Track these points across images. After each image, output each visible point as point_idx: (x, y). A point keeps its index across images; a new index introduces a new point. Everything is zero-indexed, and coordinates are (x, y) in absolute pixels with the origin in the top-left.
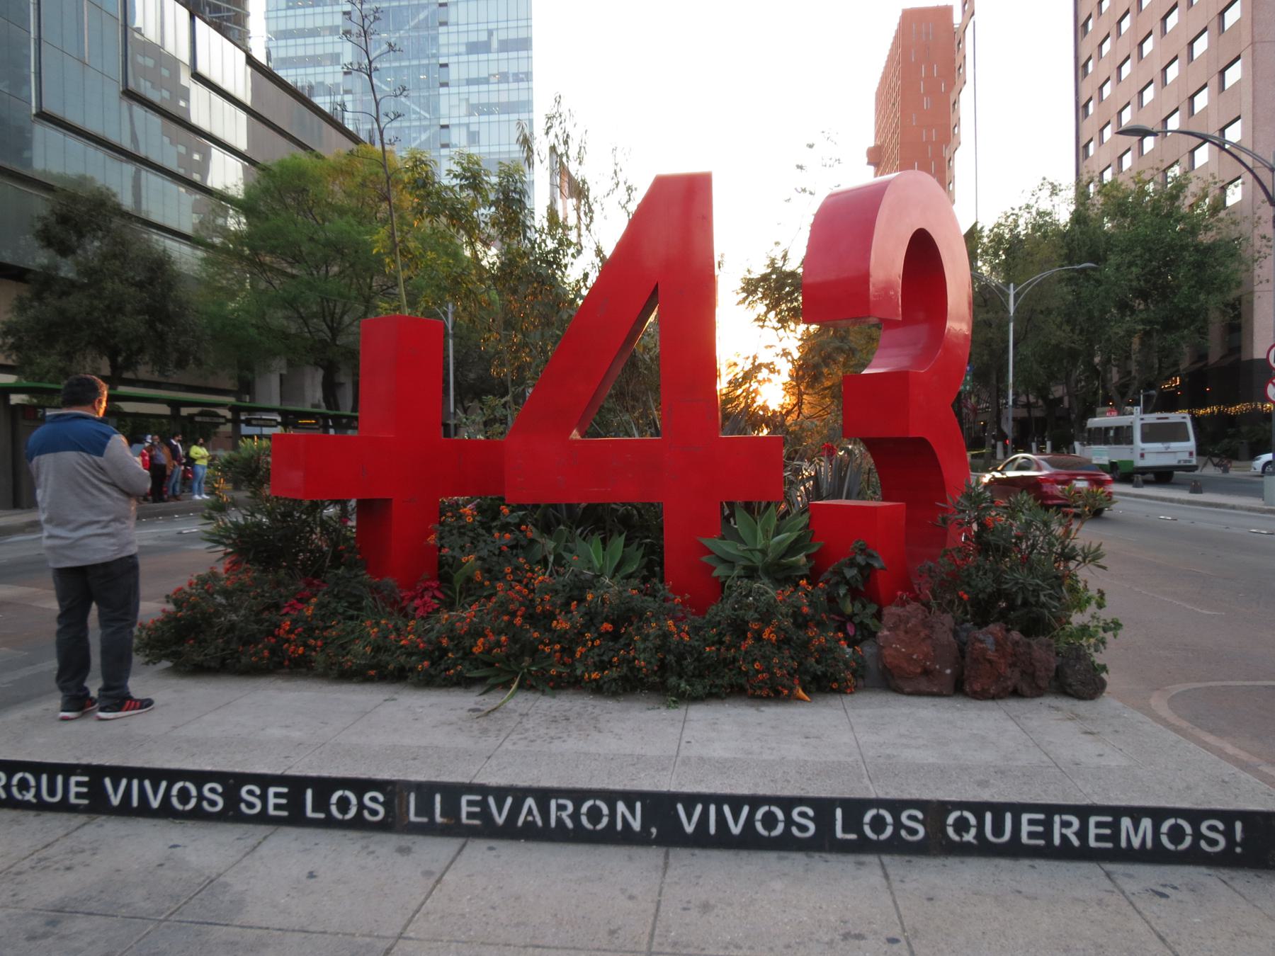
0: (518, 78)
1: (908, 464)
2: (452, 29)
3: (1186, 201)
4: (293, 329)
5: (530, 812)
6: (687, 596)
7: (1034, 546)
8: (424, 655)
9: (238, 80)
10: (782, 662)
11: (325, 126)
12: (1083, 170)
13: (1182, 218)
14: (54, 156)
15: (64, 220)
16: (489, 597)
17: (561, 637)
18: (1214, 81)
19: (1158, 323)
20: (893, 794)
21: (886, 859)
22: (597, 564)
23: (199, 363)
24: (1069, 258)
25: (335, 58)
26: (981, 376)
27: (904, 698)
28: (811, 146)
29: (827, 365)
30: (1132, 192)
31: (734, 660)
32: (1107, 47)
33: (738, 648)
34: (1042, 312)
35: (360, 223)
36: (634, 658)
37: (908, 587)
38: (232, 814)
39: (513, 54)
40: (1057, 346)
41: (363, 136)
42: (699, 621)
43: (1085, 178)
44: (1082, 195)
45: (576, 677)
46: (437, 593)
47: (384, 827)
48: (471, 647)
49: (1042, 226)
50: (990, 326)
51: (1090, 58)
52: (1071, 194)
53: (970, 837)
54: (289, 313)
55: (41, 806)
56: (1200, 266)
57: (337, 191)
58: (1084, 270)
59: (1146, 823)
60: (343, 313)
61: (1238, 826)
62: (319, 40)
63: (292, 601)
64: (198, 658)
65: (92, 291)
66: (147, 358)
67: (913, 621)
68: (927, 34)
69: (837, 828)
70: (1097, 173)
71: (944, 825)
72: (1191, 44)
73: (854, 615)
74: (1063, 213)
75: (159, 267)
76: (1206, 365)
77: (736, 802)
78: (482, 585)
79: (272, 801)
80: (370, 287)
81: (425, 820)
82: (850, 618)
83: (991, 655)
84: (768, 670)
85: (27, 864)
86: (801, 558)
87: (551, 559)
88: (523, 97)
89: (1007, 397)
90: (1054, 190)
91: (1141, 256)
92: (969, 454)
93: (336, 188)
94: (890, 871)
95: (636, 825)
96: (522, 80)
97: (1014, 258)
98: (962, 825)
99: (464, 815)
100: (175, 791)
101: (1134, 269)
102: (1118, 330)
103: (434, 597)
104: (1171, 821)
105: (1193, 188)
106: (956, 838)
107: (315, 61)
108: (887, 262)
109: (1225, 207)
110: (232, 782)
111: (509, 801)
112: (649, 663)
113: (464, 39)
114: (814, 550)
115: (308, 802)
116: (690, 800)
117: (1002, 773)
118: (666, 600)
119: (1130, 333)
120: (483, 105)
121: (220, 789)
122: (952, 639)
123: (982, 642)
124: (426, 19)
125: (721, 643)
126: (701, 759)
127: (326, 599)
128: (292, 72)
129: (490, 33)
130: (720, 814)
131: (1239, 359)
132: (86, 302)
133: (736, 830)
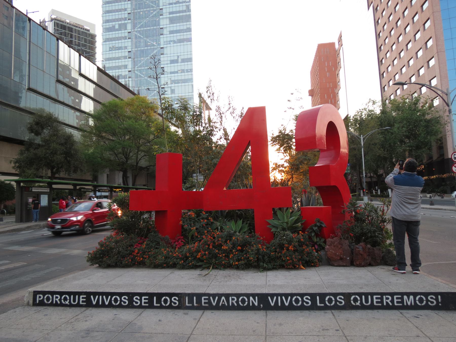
0: (187, 71)
1: (330, 193)
2: (165, 56)
3: (420, 105)
4: (112, 158)
5: (223, 301)
6: (264, 237)
7: (372, 219)
8: (181, 259)
9: (93, 74)
10: (296, 257)
11: (123, 89)
12: (383, 96)
13: (419, 111)
14: (30, 102)
15: (37, 124)
16: (200, 241)
17: (225, 251)
18: (426, 65)
19: (414, 147)
20: (334, 291)
21: (333, 311)
22: (234, 229)
23: (81, 170)
24: (381, 125)
25: (126, 67)
26: (353, 167)
27: (335, 267)
28: (292, 94)
29: (301, 165)
30: (401, 103)
31: (281, 256)
32: (388, 55)
33: (281, 253)
34: (373, 144)
35: (136, 122)
36: (249, 257)
37: (334, 233)
38: (131, 306)
39: (186, 63)
40: (379, 156)
41: (136, 92)
42: (268, 245)
43: (384, 98)
44: (384, 104)
45: (230, 264)
46: (183, 240)
47: (178, 308)
48: (196, 256)
49: (371, 115)
50: (355, 150)
51: (383, 58)
52: (380, 103)
53: (358, 304)
54: (111, 153)
55: (71, 306)
56: (427, 127)
57: (128, 112)
58: (386, 129)
59: (411, 297)
60: (130, 152)
61: (439, 297)
62: (120, 61)
63: (137, 244)
64: (109, 262)
65: (46, 147)
66: (63, 170)
67: (336, 243)
68: (327, 52)
69: (317, 302)
70: (388, 97)
71: (350, 300)
72: (417, 53)
73: (317, 242)
74: (378, 110)
75: (69, 137)
76: (432, 161)
77: (286, 295)
78: (197, 237)
79: (143, 301)
80: (140, 143)
81: (191, 305)
82: (316, 243)
83: (361, 252)
84: (291, 259)
85: (73, 320)
86: (299, 224)
87: (219, 228)
88: (190, 77)
89: (363, 175)
90: (374, 103)
91: (406, 124)
92: (351, 195)
93: (128, 110)
94: (335, 314)
95: (256, 304)
96: (189, 72)
97: (362, 126)
98: (355, 300)
99: (203, 303)
100: (113, 299)
101: (404, 129)
102: (400, 150)
103: (182, 241)
104: (419, 296)
105: (422, 100)
106: (354, 304)
107: (119, 68)
108: (321, 130)
109: (433, 107)
110: (131, 295)
111: (217, 298)
112: (254, 258)
113: (169, 59)
114: (303, 222)
115: (154, 301)
116: (272, 295)
117: (367, 285)
118: (258, 238)
119: (405, 151)
120: (176, 80)
121: (127, 298)
122: (349, 248)
123: (358, 248)
124: (156, 52)
125: (276, 251)
126: (274, 285)
127: (149, 242)
128: (111, 71)
129: (178, 57)
130: (103, 298)
131: (444, 158)
132: (44, 151)
133: (287, 304)
